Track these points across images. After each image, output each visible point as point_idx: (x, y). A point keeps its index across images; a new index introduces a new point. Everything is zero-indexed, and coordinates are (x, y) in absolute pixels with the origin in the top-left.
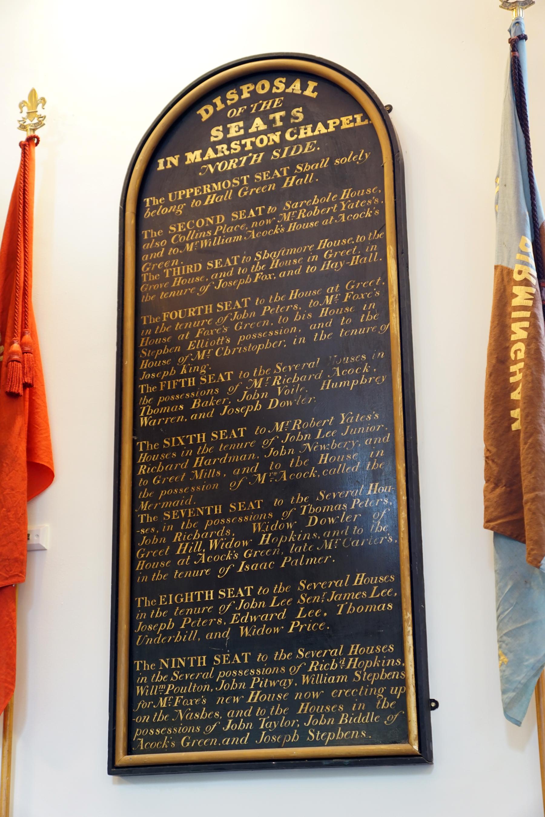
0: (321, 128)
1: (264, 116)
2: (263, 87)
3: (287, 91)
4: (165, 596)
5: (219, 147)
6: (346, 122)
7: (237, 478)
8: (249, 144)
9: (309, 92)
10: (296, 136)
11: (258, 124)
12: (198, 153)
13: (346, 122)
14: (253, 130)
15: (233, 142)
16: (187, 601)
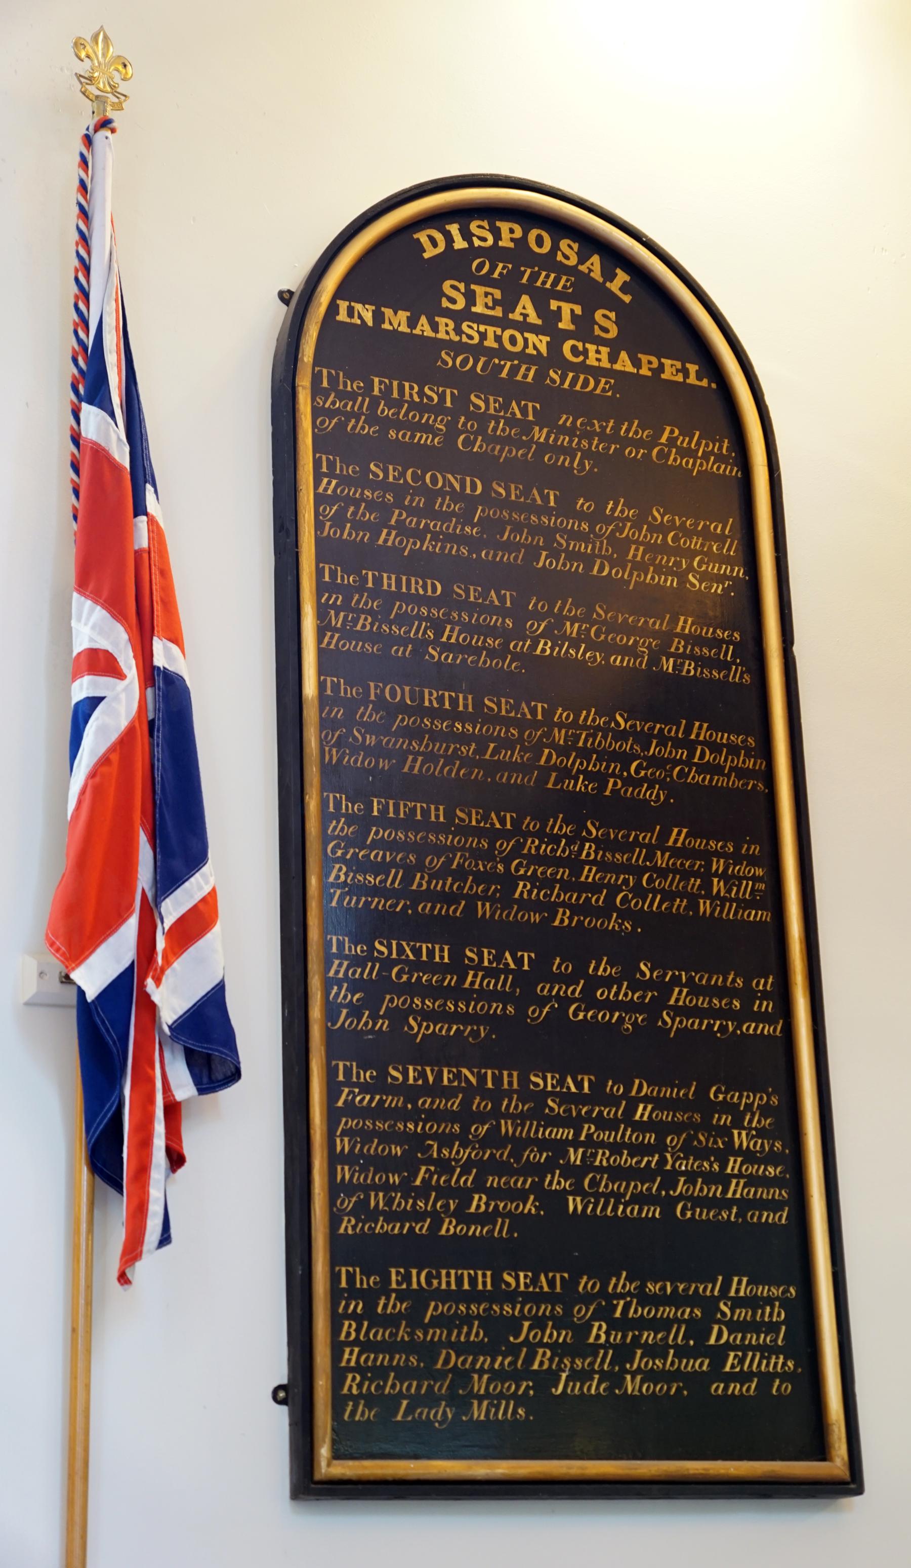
0: (624, 363)
1: (541, 300)
2: (540, 242)
3: (581, 268)
4: (402, 1270)
5: (442, 321)
6: (671, 370)
7: (542, 1002)
8: (490, 335)
9: (615, 286)
10: (581, 358)
11: (526, 307)
12: (403, 315)
13: (671, 370)
14: (516, 316)
15: (470, 319)
16: (444, 1286)
